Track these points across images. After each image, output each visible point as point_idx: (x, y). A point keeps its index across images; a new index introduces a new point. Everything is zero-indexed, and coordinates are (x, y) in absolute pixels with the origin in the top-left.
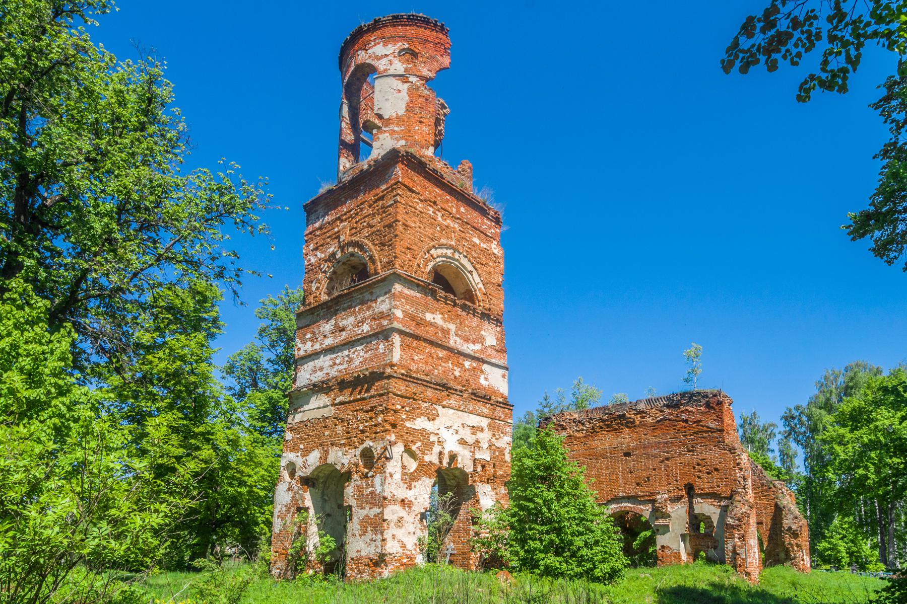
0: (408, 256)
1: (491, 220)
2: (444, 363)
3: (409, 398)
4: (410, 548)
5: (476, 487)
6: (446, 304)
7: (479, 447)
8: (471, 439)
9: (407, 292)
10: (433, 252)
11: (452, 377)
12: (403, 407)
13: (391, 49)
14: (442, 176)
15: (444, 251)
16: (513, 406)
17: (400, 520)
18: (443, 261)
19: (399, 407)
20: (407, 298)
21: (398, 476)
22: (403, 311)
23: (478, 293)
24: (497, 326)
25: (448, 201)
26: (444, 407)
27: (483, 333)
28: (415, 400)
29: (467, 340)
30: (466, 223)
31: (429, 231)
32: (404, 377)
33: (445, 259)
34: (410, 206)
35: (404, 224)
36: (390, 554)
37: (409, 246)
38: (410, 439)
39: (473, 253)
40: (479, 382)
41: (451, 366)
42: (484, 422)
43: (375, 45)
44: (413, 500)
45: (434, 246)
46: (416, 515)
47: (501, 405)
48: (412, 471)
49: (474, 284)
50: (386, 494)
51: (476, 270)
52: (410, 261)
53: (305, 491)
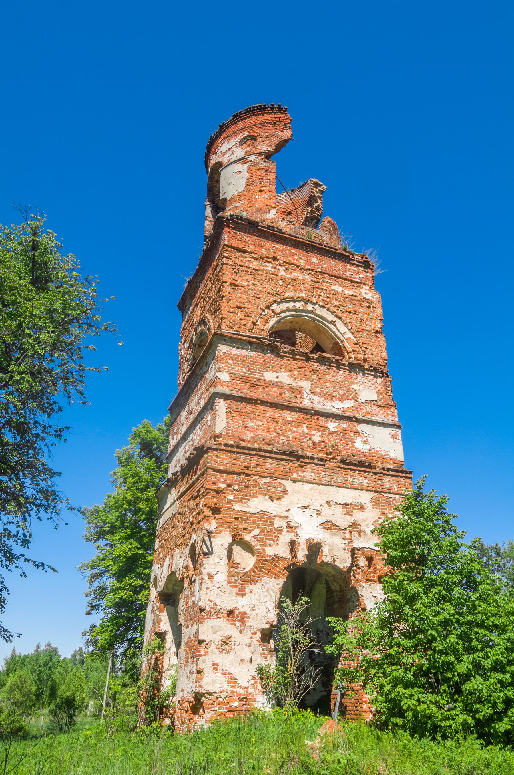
0: (239, 315)
1: (358, 266)
2: (296, 427)
3: (239, 474)
4: (245, 685)
5: (359, 589)
6: (296, 360)
7: (359, 532)
8: (343, 521)
9: (235, 351)
10: (274, 307)
11: (310, 443)
12: (229, 486)
13: (234, 141)
14: (280, 231)
15: (291, 305)
16: (411, 473)
17: (226, 641)
18: (292, 316)
19: (223, 486)
20: (235, 359)
21: (221, 577)
22: (229, 373)
23: (346, 344)
24: (376, 377)
25: (293, 254)
26: (295, 482)
27: (353, 387)
28: (247, 475)
29: (331, 397)
30: (321, 273)
31: (269, 287)
32: (229, 449)
33: (295, 313)
34: (240, 266)
35: (231, 284)
36: (210, 694)
37: (239, 305)
38: (242, 526)
39: (334, 302)
40: (353, 446)
41: (306, 430)
42: (365, 498)
43: (222, 145)
44: (248, 611)
45: (275, 301)
46: (255, 633)
47: (391, 473)
48: (247, 570)
49: (339, 335)
50: (201, 604)
51: (340, 319)
52: (241, 320)
53: (161, 611)
